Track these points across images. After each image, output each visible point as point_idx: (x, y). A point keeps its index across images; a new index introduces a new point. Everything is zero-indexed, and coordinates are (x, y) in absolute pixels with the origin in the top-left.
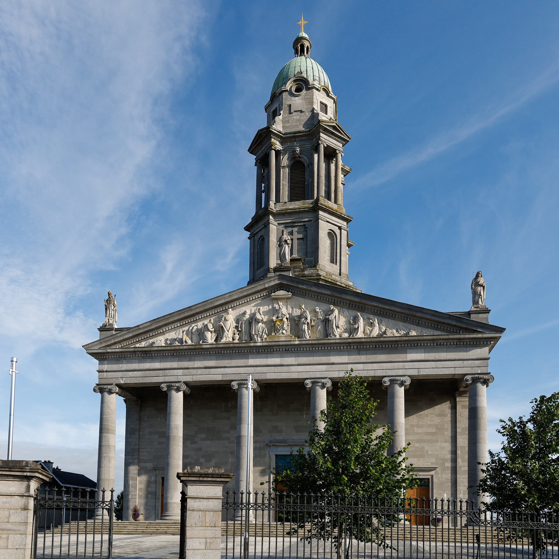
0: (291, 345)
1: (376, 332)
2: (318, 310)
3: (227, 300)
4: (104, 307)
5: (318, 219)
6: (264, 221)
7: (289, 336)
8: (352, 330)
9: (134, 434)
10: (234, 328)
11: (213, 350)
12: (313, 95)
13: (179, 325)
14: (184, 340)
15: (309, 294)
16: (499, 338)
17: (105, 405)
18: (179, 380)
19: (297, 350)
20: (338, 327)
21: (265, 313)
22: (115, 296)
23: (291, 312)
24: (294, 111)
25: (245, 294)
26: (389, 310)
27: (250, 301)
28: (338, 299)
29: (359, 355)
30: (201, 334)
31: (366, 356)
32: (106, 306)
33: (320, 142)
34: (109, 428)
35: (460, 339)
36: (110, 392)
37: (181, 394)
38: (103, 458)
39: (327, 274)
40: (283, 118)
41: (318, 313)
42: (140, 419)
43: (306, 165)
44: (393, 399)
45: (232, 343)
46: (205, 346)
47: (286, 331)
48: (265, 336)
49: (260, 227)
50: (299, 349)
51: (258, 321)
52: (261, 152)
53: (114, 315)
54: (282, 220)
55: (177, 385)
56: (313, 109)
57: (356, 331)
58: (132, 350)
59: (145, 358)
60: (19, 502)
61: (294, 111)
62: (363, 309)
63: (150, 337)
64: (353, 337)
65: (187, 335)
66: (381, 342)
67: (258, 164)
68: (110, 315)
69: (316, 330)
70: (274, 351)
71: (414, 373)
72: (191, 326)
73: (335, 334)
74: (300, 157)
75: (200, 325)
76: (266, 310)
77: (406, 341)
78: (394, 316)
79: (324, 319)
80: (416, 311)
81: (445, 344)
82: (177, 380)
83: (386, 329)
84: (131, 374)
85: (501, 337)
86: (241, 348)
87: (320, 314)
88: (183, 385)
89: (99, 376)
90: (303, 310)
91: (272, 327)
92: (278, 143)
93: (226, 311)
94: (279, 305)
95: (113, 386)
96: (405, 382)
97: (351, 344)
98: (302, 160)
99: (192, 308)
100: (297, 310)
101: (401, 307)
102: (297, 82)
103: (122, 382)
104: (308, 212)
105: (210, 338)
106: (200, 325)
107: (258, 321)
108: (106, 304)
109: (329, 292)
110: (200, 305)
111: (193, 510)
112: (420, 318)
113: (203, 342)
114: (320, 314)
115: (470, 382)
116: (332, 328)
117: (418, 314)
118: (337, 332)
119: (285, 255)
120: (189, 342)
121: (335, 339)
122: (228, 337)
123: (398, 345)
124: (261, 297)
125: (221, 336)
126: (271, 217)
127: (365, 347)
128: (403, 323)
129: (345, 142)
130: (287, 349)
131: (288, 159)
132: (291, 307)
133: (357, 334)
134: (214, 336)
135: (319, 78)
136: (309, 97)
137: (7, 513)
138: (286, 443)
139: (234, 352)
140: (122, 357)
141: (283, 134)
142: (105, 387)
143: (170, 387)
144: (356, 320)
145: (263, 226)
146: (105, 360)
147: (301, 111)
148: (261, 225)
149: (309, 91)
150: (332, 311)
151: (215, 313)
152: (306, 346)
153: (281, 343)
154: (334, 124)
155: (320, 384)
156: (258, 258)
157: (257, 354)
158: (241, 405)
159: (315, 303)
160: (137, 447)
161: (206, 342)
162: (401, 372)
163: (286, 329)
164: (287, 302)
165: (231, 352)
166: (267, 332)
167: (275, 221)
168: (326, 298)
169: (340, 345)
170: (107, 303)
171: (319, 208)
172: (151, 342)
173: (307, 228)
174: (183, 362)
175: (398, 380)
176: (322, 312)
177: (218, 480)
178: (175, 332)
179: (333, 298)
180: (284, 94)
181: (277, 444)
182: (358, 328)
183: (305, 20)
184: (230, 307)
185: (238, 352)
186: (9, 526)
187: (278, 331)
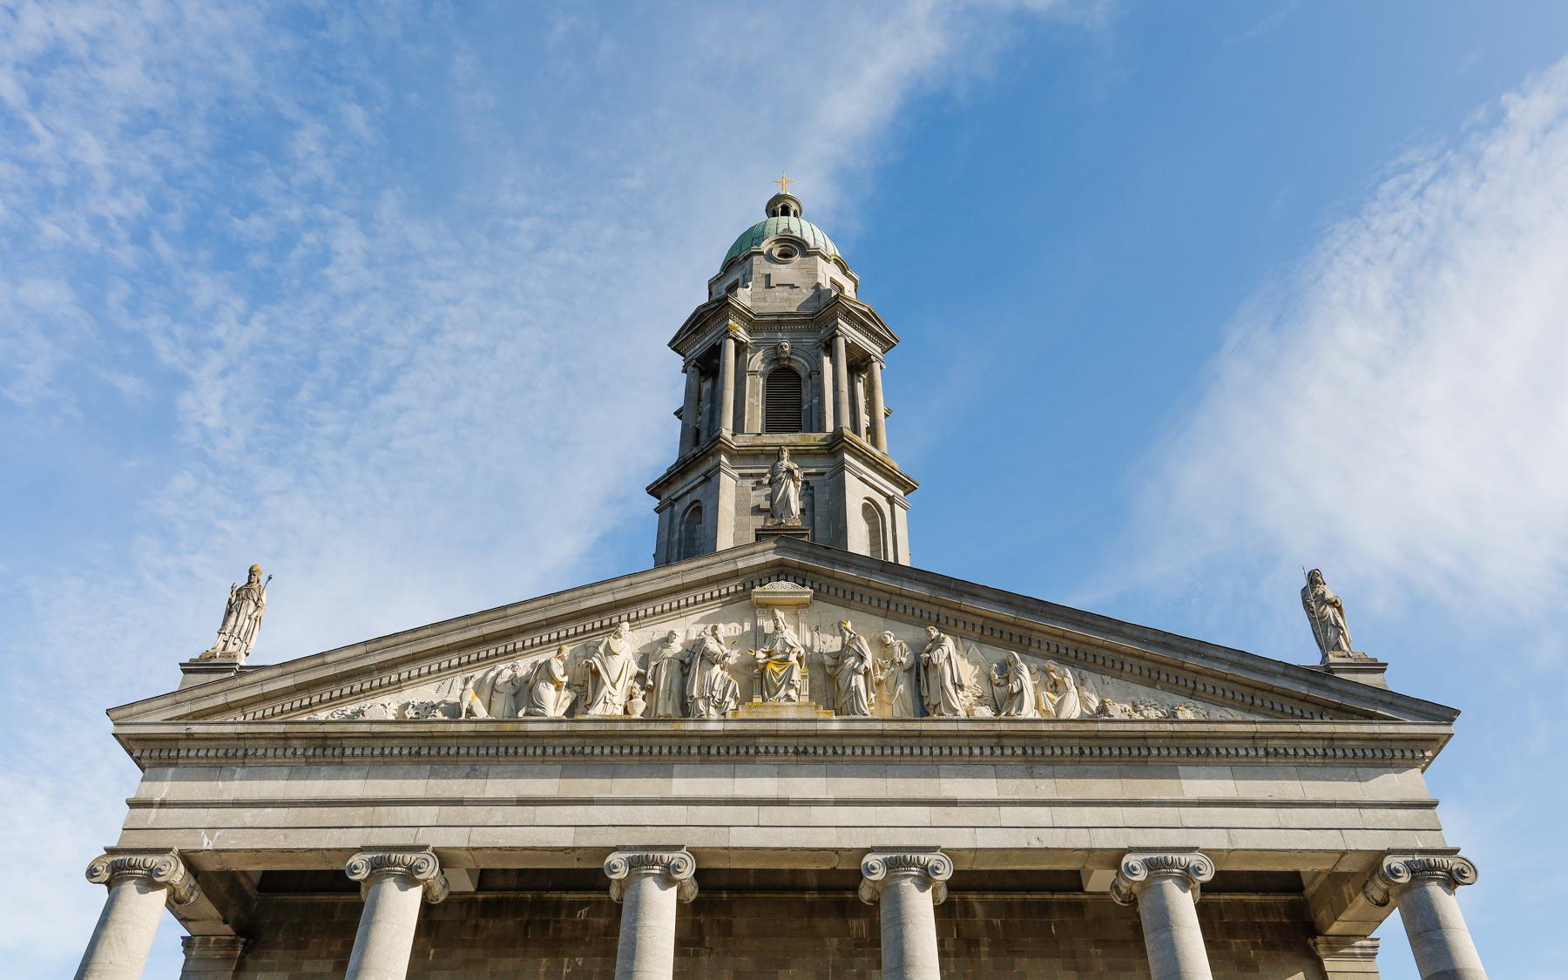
0: (816, 735)
1: (1073, 708)
2: (890, 640)
3: (619, 596)
8: (1003, 698)
10: (631, 678)
11: (555, 742)
13: (455, 662)
14: (465, 706)
15: (861, 596)
16: (1446, 742)
17: (111, 932)
18: (421, 843)
19: (835, 753)
20: (961, 687)
21: (733, 642)
22: (270, 578)
23: (809, 645)
25: (676, 581)
26: (1102, 647)
27: (687, 605)
28: (949, 613)
29: (1032, 777)
30: (524, 692)
31: (1052, 780)
32: (231, 606)
37: (415, 895)
41: (893, 648)
43: (803, 374)
44: (1170, 931)
45: (622, 721)
46: (531, 727)
47: (799, 695)
48: (732, 705)
49: (691, 482)
50: (840, 751)
51: (710, 660)
52: (699, 347)
53: (247, 632)
54: (751, 468)
55: (409, 858)
56: (818, 284)
57: (1016, 702)
59: (317, 764)
62: (1025, 642)
63: (351, 694)
64: (1010, 718)
65: (478, 692)
66: (1097, 736)
67: (690, 368)
68: (237, 630)
69: (892, 696)
70: (757, 752)
72: (493, 669)
73: (955, 707)
74: (789, 359)
75: (524, 666)
76: (737, 634)
77: (1172, 737)
78: (1118, 666)
79: (913, 666)
80: (1187, 652)
82: (410, 842)
83: (1103, 702)
84: (249, 816)
85: (1450, 736)
87: (897, 649)
89: (130, 818)
90: (848, 634)
91: (756, 681)
92: (742, 330)
93: (613, 629)
94: (777, 620)
95: (167, 857)
96: (1197, 870)
97: (1005, 742)
98: (793, 365)
99: (510, 611)
101: (1137, 640)
103: (207, 842)
104: (816, 454)
105: (554, 702)
106: (524, 666)
107: (710, 660)
108: (233, 601)
109: (923, 589)
110: (536, 604)
112: (1197, 672)
113: (527, 714)
114: (897, 649)
115: (1405, 878)
116: (943, 688)
117: (1193, 662)
118: (961, 702)
119: (788, 501)
121: (957, 721)
124: (720, 596)
125: (589, 701)
126: (723, 458)
128: (1147, 689)
129: (887, 344)
130: (801, 749)
131: (762, 361)
132: (809, 628)
133: (1020, 708)
134: (566, 698)
139: (626, 751)
140: (235, 755)
141: (755, 315)
142: (135, 859)
144: (1007, 671)
145: (703, 478)
146: (169, 765)
147: (792, 286)
148: (694, 477)
149: (807, 259)
150: (938, 643)
151: (576, 634)
152: (864, 741)
153: (783, 726)
155: (915, 871)
157: (702, 762)
158: (633, 944)
159: (881, 621)
161: (537, 714)
163: (798, 687)
164: (796, 614)
165: (617, 751)
166: (738, 691)
167: (733, 468)
168: (913, 609)
169: (971, 740)
170: (238, 595)
171: (844, 447)
172: (349, 712)
173: (812, 488)
174: (445, 781)
175: (1172, 865)
176: (904, 646)
178: (437, 684)
179: (935, 609)
180: (756, 259)
182: (1021, 691)
184: (624, 617)
185: (641, 753)
187: (773, 691)
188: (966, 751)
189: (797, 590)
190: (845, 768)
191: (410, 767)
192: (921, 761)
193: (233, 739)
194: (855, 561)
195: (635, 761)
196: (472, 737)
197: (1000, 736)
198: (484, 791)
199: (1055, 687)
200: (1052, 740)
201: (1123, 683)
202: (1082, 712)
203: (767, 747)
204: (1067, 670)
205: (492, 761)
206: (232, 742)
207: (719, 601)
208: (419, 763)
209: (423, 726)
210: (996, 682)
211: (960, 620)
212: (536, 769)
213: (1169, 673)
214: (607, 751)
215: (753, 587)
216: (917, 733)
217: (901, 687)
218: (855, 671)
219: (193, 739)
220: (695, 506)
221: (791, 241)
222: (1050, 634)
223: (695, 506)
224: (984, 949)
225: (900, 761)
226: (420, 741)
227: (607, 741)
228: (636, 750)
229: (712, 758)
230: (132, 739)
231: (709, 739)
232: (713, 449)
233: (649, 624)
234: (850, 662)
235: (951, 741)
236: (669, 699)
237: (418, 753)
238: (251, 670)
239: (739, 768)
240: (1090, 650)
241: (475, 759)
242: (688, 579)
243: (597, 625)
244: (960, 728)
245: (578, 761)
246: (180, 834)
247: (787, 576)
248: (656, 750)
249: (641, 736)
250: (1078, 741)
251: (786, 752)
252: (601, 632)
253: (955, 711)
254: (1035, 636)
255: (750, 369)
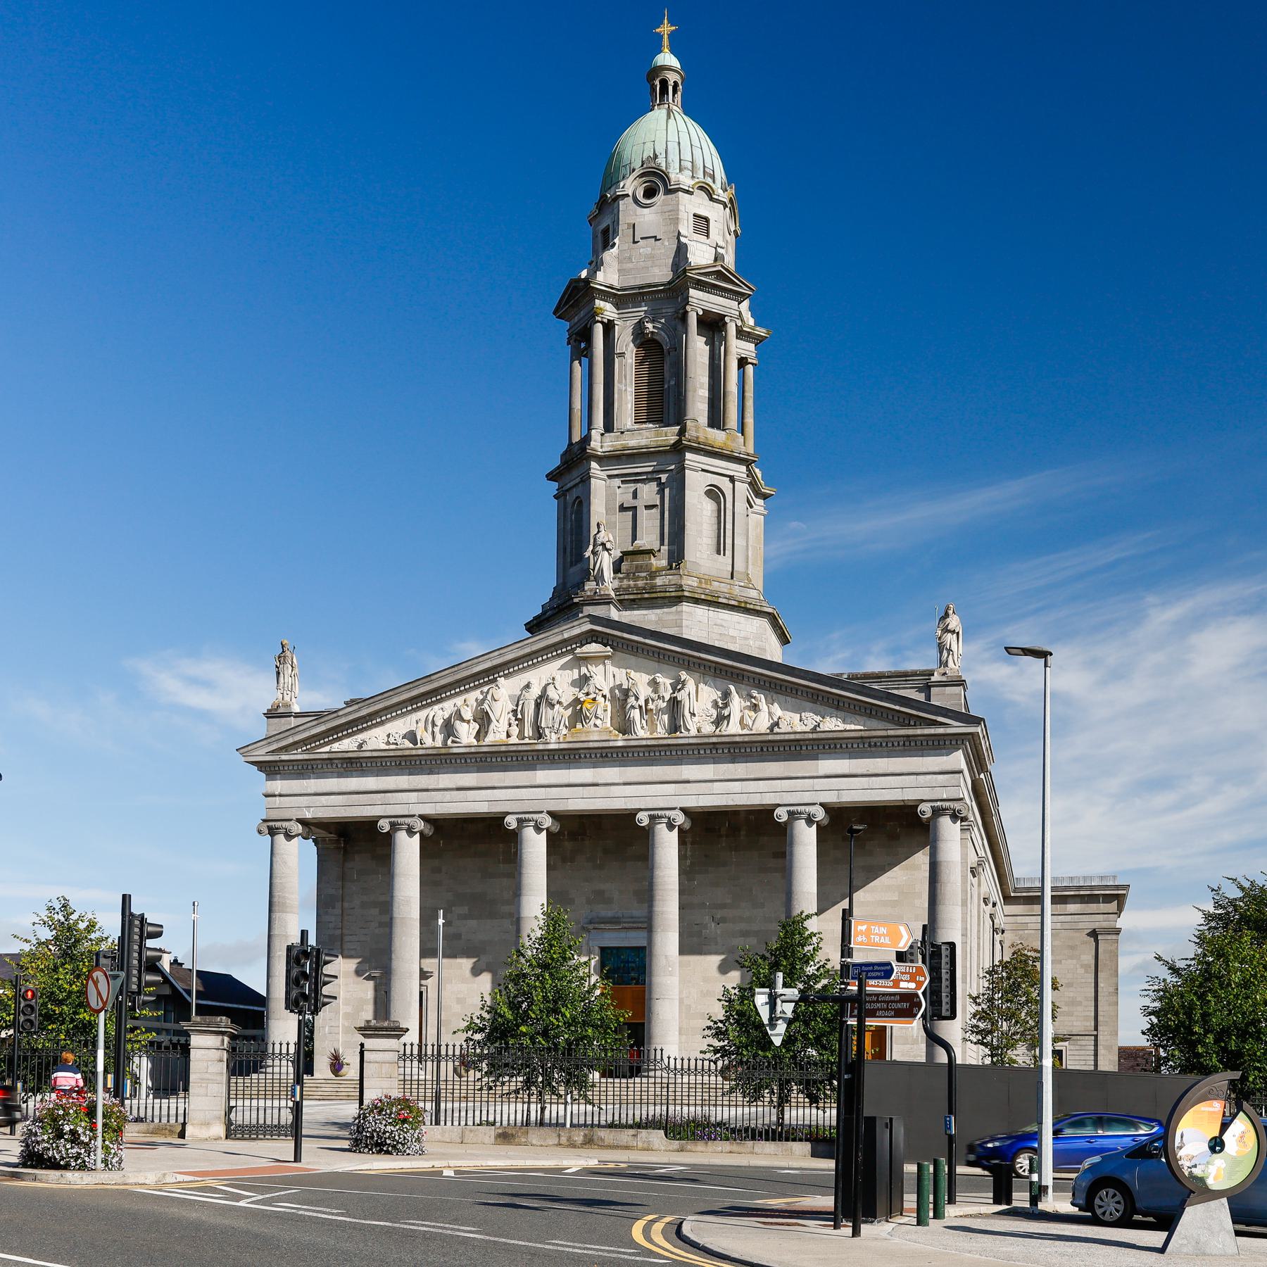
4: (275, 670)
5: (684, 469)
6: (582, 470)
9: (334, 908)
11: (471, 756)
12: (678, 204)
20: (694, 715)
24: (642, 238)
25: (527, 650)
30: (449, 729)
33: (688, 308)
34: (285, 903)
35: (908, 736)
36: (289, 837)
38: (277, 959)
39: (700, 582)
40: (621, 251)
42: (343, 878)
46: (455, 751)
57: (726, 722)
58: (326, 756)
60: (217, 1054)
61: (642, 238)
70: (580, 757)
71: (830, 798)
81: (884, 744)
82: (406, 813)
86: (522, 754)
90: (631, 680)
91: (578, 714)
102: (642, 177)
105: (466, 734)
111: (370, 1062)
113: (453, 742)
120: (429, 742)
122: (497, 734)
123: (801, 746)
126: (594, 465)
127: (743, 750)
135: (692, 163)
136: (670, 208)
137: (205, 1064)
138: (619, 923)
143: (395, 827)
144: (726, 695)
146: (277, 774)
153: (591, 745)
156: (572, 542)
160: (339, 932)
162: (807, 798)
165: (504, 760)
177: (392, 1033)
181: (602, 926)
183: (671, 23)
186: (207, 1076)
187: (587, 721)
188: (696, 752)
198: (438, 783)
199: (755, 708)
201: (798, 701)
214: (499, 759)
218: (633, 707)
221: (654, 174)
224: (743, 833)
237: (400, 764)
242: (535, 648)
246: (294, 810)
248: (525, 759)
251: (596, 756)
255: (618, 352)
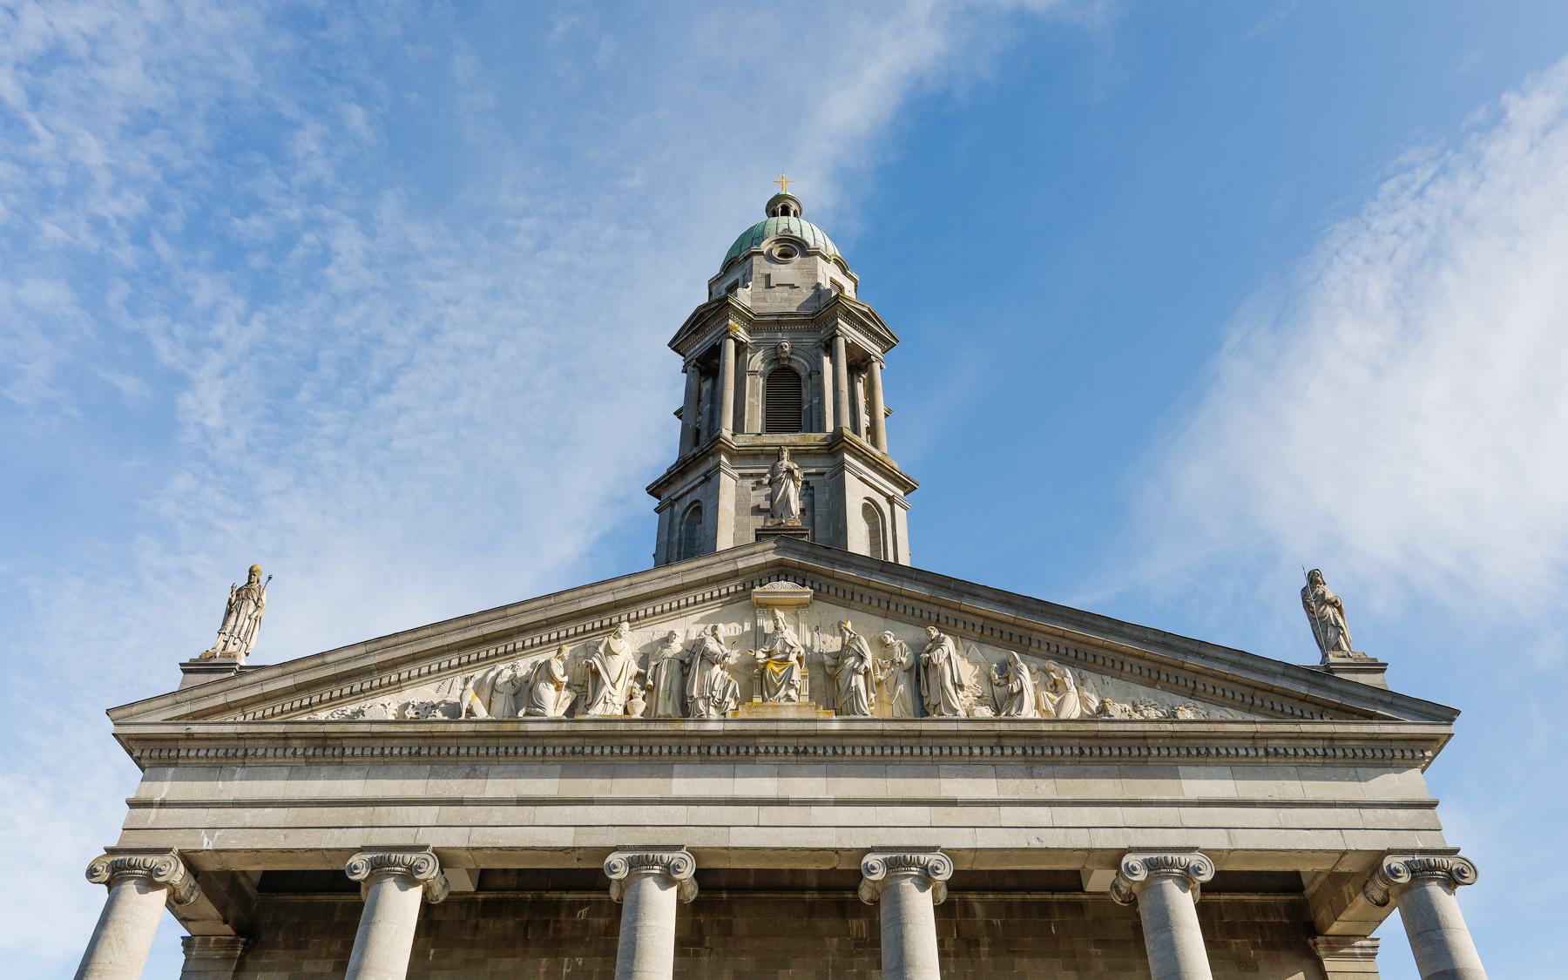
0: (816, 735)
1: (1073, 708)
2: (890, 640)
3: (619, 596)
7: (807, 705)
8: (1003, 698)
10: (631, 678)
11: (555, 742)
13: (455, 662)
14: (465, 706)
15: (861, 596)
16: (1446, 742)
17: (111, 932)
18: (421, 843)
19: (835, 753)
20: (961, 687)
21: (733, 642)
22: (270, 578)
23: (809, 645)
25: (676, 581)
26: (1102, 647)
27: (687, 605)
28: (949, 613)
29: (1032, 777)
30: (524, 692)
31: (1052, 780)
32: (231, 606)
37: (415, 895)
41: (893, 648)
43: (803, 374)
44: (1170, 931)
45: (622, 721)
46: (531, 727)
48: (732, 705)
49: (691, 482)
50: (840, 751)
51: (710, 660)
52: (699, 347)
53: (247, 632)
54: (751, 468)
55: (409, 858)
56: (818, 284)
57: (1016, 702)
62: (1025, 642)
63: (351, 694)
64: (1010, 718)
65: (478, 692)
66: (1097, 736)
67: (690, 368)
68: (237, 630)
69: (892, 696)
70: (757, 752)
72: (493, 669)
74: (789, 359)
75: (524, 666)
76: (737, 634)
77: (1172, 737)
78: (1118, 666)
79: (913, 666)
80: (1187, 652)
82: (410, 842)
83: (1103, 702)
84: (249, 816)
85: (1450, 736)
87: (897, 649)
88: (430, 859)
89: (130, 818)
90: (848, 634)
91: (756, 681)
92: (742, 330)
93: (613, 629)
94: (777, 620)
95: (167, 857)
96: (1197, 870)
97: (1005, 742)
98: (793, 365)
99: (510, 611)
100: (829, 638)
101: (1137, 640)
103: (207, 842)
104: (816, 454)
105: (554, 702)
106: (524, 666)
107: (710, 660)
108: (233, 601)
109: (923, 589)
110: (536, 604)
112: (1197, 672)
113: (527, 714)
114: (897, 649)
116: (943, 688)
117: (1193, 662)
118: (961, 702)
119: (788, 501)
121: (957, 721)
124: (720, 596)
125: (589, 701)
126: (723, 458)
128: (1147, 689)
129: (887, 344)
130: (801, 749)
131: (762, 361)
132: (809, 628)
133: (1020, 708)
134: (566, 698)
139: (626, 751)
140: (235, 755)
141: (755, 315)
142: (135, 859)
144: (1007, 671)
145: (703, 478)
146: (169, 765)
147: (792, 286)
148: (694, 477)
149: (807, 259)
150: (938, 643)
151: (576, 634)
152: (864, 741)
153: (783, 726)
154: (866, 310)
155: (915, 871)
157: (702, 762)
158: (633, 944)
159: (881, 621)
161: (537, 714)
163: (798, 687)
164: (796, 614)
165: (617, 751)
166: (738, 691)
167: (733, 468)
168: (913, 609)
169: (971, 740)
171: (844, 447)
172: (349, 712)
173: (812, 488)
174: (445, 781)
175: (1172, 865)
176: (904, 646)
178: (437, 684)
179: (935, 609)
180: (756, 259)
182: (1021, 691)
184: (624, 617)
185: (641, 753)
187: (773, 691)
188: (966, 751)
189: (797, 590)
190: (845, 768)
191: (410, 767)
192: (921, 761)
193: (233, 739)
194: (855, 561)
195: (635, 761)
196: (472, 737)
197: (1000, 736)
198: (484, 791)
199: (1055, 687)
200: (1052, 740)
201: (1123, 683)
202: (1082, 712)
203: (767, 747)
204: (1067, 670)
205: (492, 761)
206: (232, 742)
207: (719, 601)
208: (419, 763)
209: (423, 726)
210: (996, 682)
211: (960, 620)
212: (536, 769)
213: (1169, 673)
214: (607, 751)
215: (753, 587)
216: (917, 733)
217: (901, 687)
218: (855, 671)
219: (193, 739)
220: (695, 506)
221: (791, 241)
222: (1050, 634)
223: (695, 506)
224: (984, 949)
225: (900, 761)
226: (420, 741)
227: (607, 741)
228: (636, 750)
229: (712, 758)
230: (132, 739)
231: (709, 739)
232: (713, 449)
233: (649, 624)
234: (850, 662)
235: (951, 741)
236: (669, 699)
237: (418, 753)
238: (251, 670)
239: (739, 768)
240: (1090, 650)
241: (475, 759)
242: (688, 579)
243: (597, 625)
244: (960, 728)
245: (578, 761)
246: (180, 834)
247: (787, 576)
248: (656, 750)
249: (641, 736)
250: (1078, 741)
251: (786, 752)
252: (601, 632)
253: (955, 711)
254: (1035, 636)
255: (750, 369)
